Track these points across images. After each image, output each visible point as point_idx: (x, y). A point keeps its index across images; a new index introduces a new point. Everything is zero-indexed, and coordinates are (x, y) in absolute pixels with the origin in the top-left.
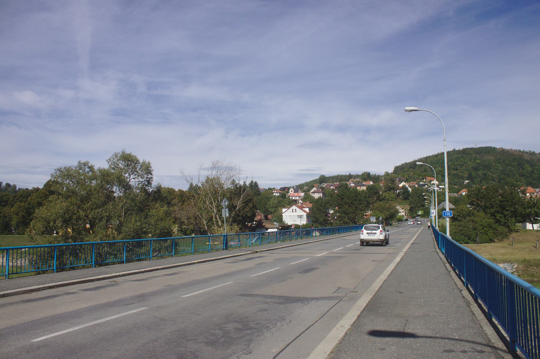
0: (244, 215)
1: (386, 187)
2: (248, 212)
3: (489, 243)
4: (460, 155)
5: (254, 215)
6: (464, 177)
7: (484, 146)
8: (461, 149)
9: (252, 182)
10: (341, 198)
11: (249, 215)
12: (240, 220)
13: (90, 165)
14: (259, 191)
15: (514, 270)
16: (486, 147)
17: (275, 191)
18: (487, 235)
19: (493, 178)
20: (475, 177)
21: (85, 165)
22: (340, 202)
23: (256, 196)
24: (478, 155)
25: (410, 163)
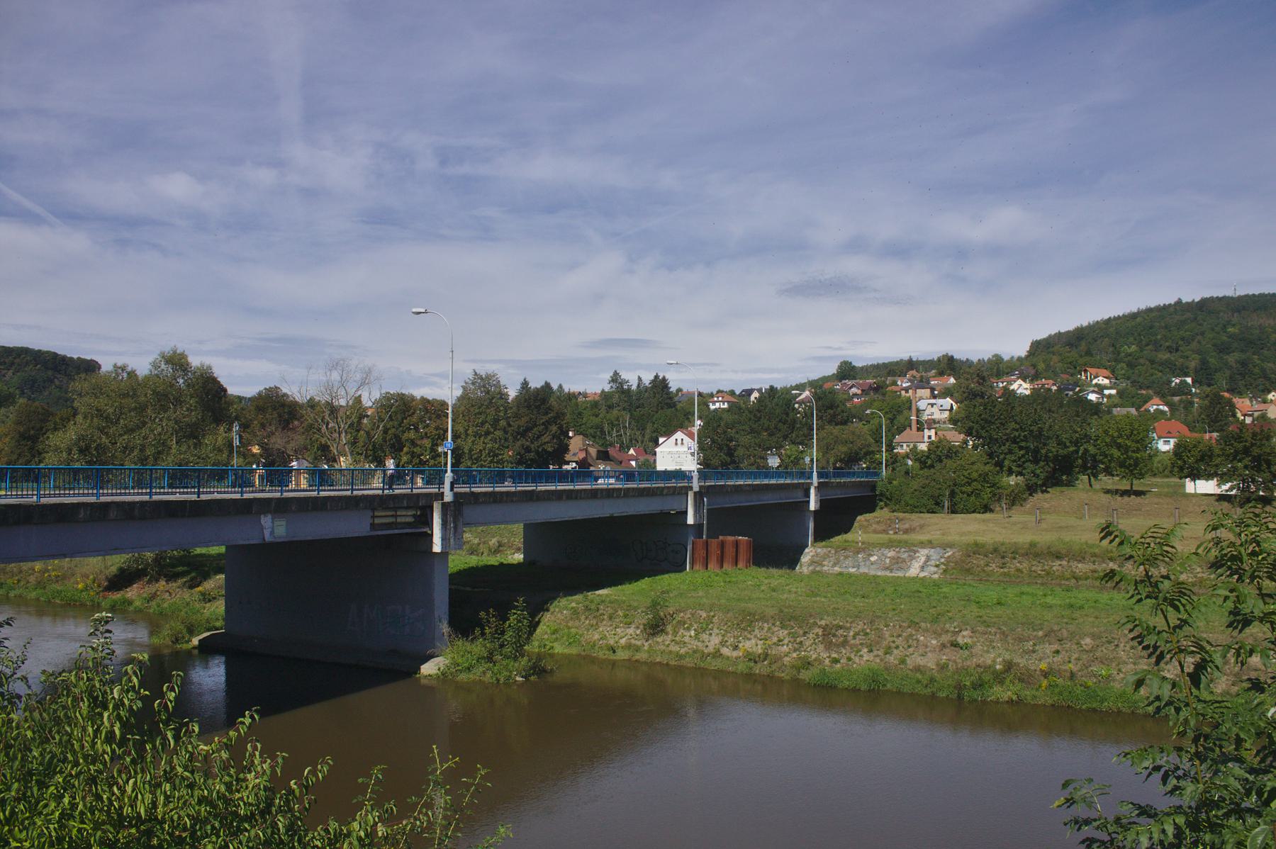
0: (540, 450)
1: (964, 392)
2: (547, 443)
3: (980, 513)
4: (1188, 315)
5: (565, 449)
6: (1187, 368)
7: (1257, 293)
8: (1197, 300)
9: (656, 377)
10: (755, 416)
11: (550, 449)
12: (531, 460)
13: (129, 369)
14: (671, 398)
15: (943, 560)
16: (1261, 295)
17: (718, 397)
18: (978, 496)
19: (1263, 370)
20: (1216, 369)
21: (123, 370)
22: (754, 426)
23: (662, 409)
24: (1236, 315)
25: (1068, 332)
